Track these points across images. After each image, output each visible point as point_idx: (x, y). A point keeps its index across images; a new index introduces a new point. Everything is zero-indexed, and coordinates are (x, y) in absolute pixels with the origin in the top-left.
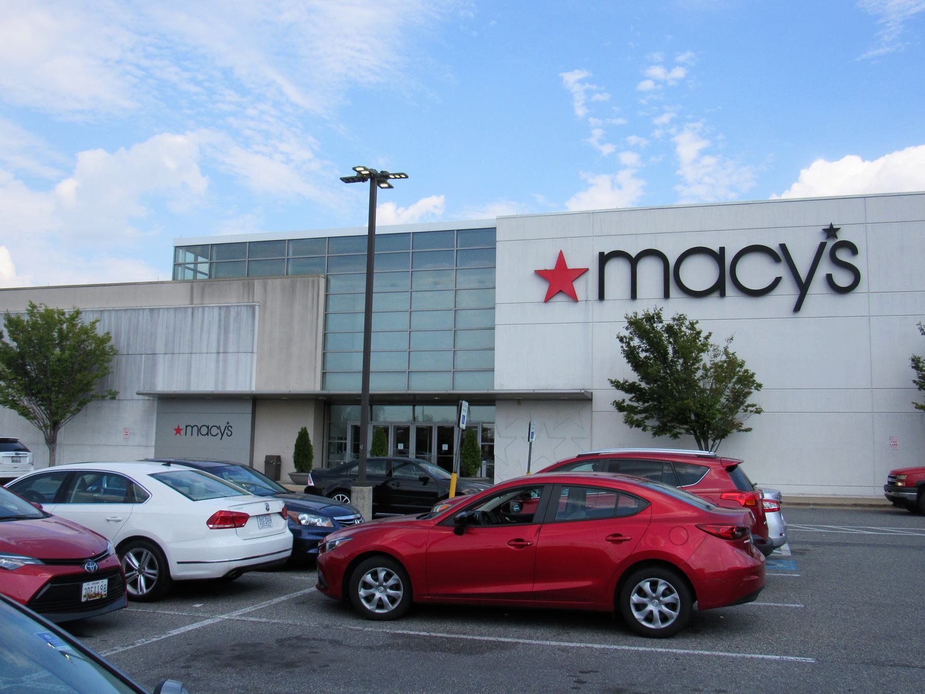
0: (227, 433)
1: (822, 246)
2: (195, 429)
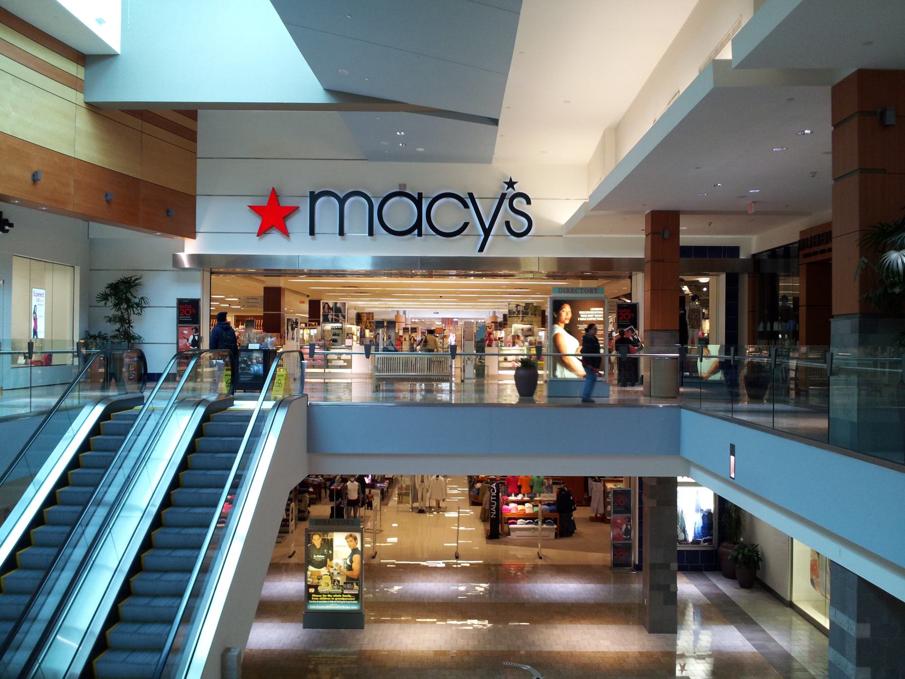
0: (507, 224)
1: (503, 196)
2: (356, 209)
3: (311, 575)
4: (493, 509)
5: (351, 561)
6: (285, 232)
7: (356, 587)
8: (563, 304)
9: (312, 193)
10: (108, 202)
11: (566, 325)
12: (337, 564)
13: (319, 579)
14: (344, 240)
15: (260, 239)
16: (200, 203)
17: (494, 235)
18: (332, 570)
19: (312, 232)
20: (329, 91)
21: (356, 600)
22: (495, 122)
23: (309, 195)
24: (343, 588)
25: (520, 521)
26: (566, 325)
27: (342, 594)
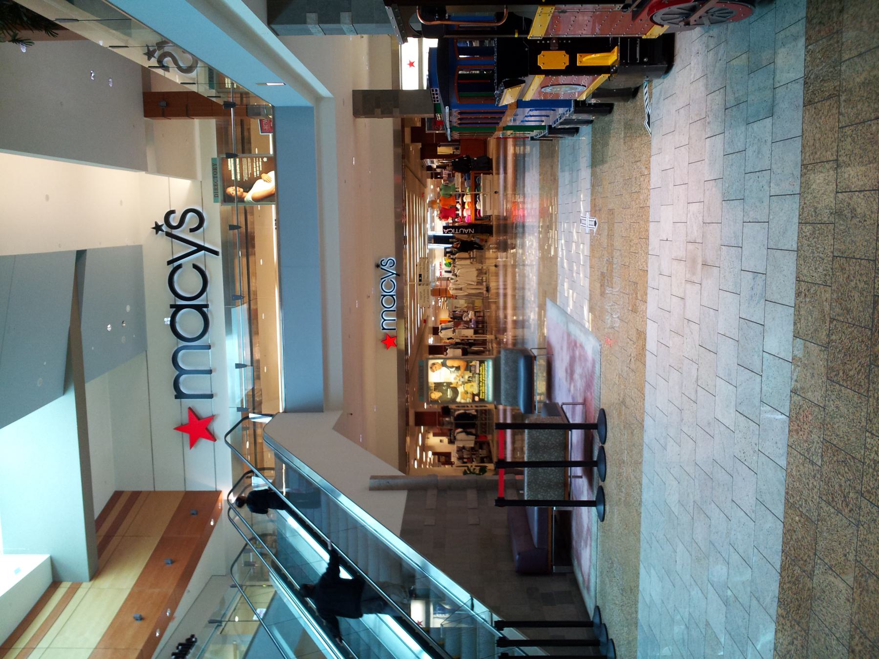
0: (192, 230)
1: (168, 234)
2: (188, 360)
3: (464, 399)
4: (466, 231)
5: (452, 367)
6: (211, 419)
7: (473, 363)
8: (227, 194)
9: (176, 397)
10: (173, 562)
11: (244, 191)
12: (455, 379)
13: (467, 393)
14: (215, 370)
15: (218, 439)
16: (190, 488)
17: (204, 241)
18: (460, 383)
19: (211, 396)
20: (65, 391)
21: (484, 363)
22: (81, 255)
23: (179, 400)
24: (475, 373)
25: (478, 207)
26: (244, 191)
27: (479, 374)
